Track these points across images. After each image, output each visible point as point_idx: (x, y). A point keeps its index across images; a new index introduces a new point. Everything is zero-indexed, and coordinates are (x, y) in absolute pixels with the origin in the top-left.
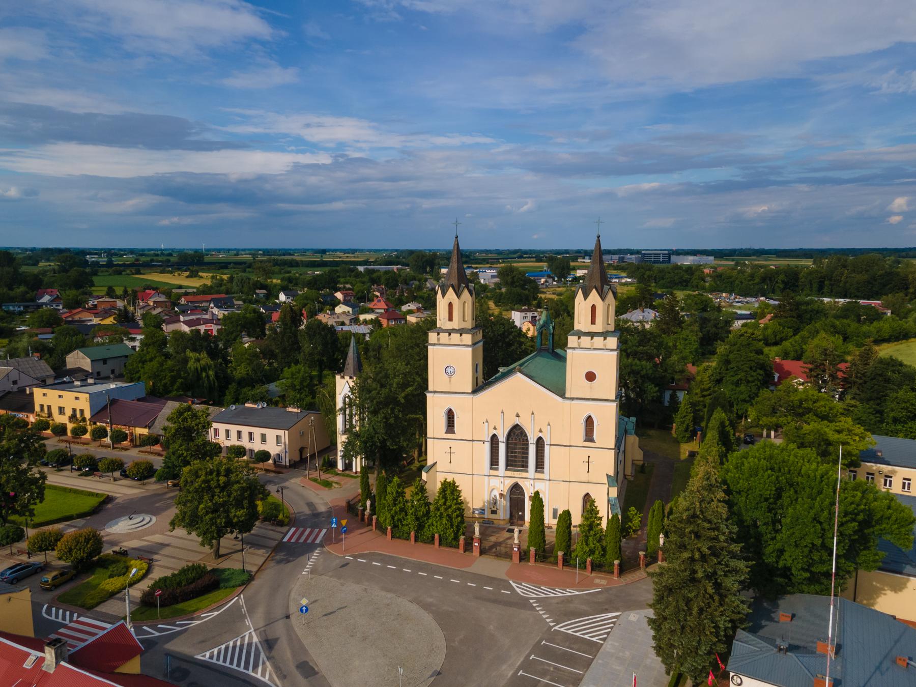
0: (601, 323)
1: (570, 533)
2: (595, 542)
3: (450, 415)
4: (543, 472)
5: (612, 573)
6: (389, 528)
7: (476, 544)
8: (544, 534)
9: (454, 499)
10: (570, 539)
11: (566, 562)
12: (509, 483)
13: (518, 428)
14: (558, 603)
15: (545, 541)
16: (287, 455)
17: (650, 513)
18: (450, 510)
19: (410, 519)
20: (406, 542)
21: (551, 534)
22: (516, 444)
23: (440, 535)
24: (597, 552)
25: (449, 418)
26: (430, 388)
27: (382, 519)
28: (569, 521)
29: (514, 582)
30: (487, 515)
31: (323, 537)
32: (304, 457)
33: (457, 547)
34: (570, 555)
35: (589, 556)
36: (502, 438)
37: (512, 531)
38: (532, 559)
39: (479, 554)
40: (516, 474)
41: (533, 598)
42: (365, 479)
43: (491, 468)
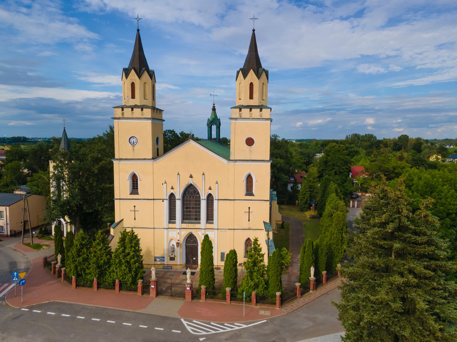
0: (258, 98)
1: (236, 270)
2: (259, 277)
3: (134, 179)
4: (212, 223)
5: (275, 304)
6: (73, 277)
7: (153, 286)
8: (213, 273)
9: (132, 247)
10: (236, 276)
11: (233, 297)
12: (185, 233)
13: (192, 187)
14: (227, 339)
15: (214, 279)
16: (8, 226)
17: (302, 250)
18: (128, 257)
19: (93, 266)
20: (89, 289)
21: (219, 274)
22: (190, 201)
23: (120, 281)
24: (261, 286)
25: (133, 181)
26: (117, 156)
27: (68, 270)
28: (235, 260)
29: (185, 320)
30: (167, 261)
31: (8, 291)
32: (26, 229)
33: (136, 290)
34: (237, 290)
35: (254, 289)
36: (178, 195)
37: (185, 273)
38: (203, 297)
39: (155, 295)
40: (191, 226)
41: (202, 336)
42: (58, 237)
43: (169, 223)
